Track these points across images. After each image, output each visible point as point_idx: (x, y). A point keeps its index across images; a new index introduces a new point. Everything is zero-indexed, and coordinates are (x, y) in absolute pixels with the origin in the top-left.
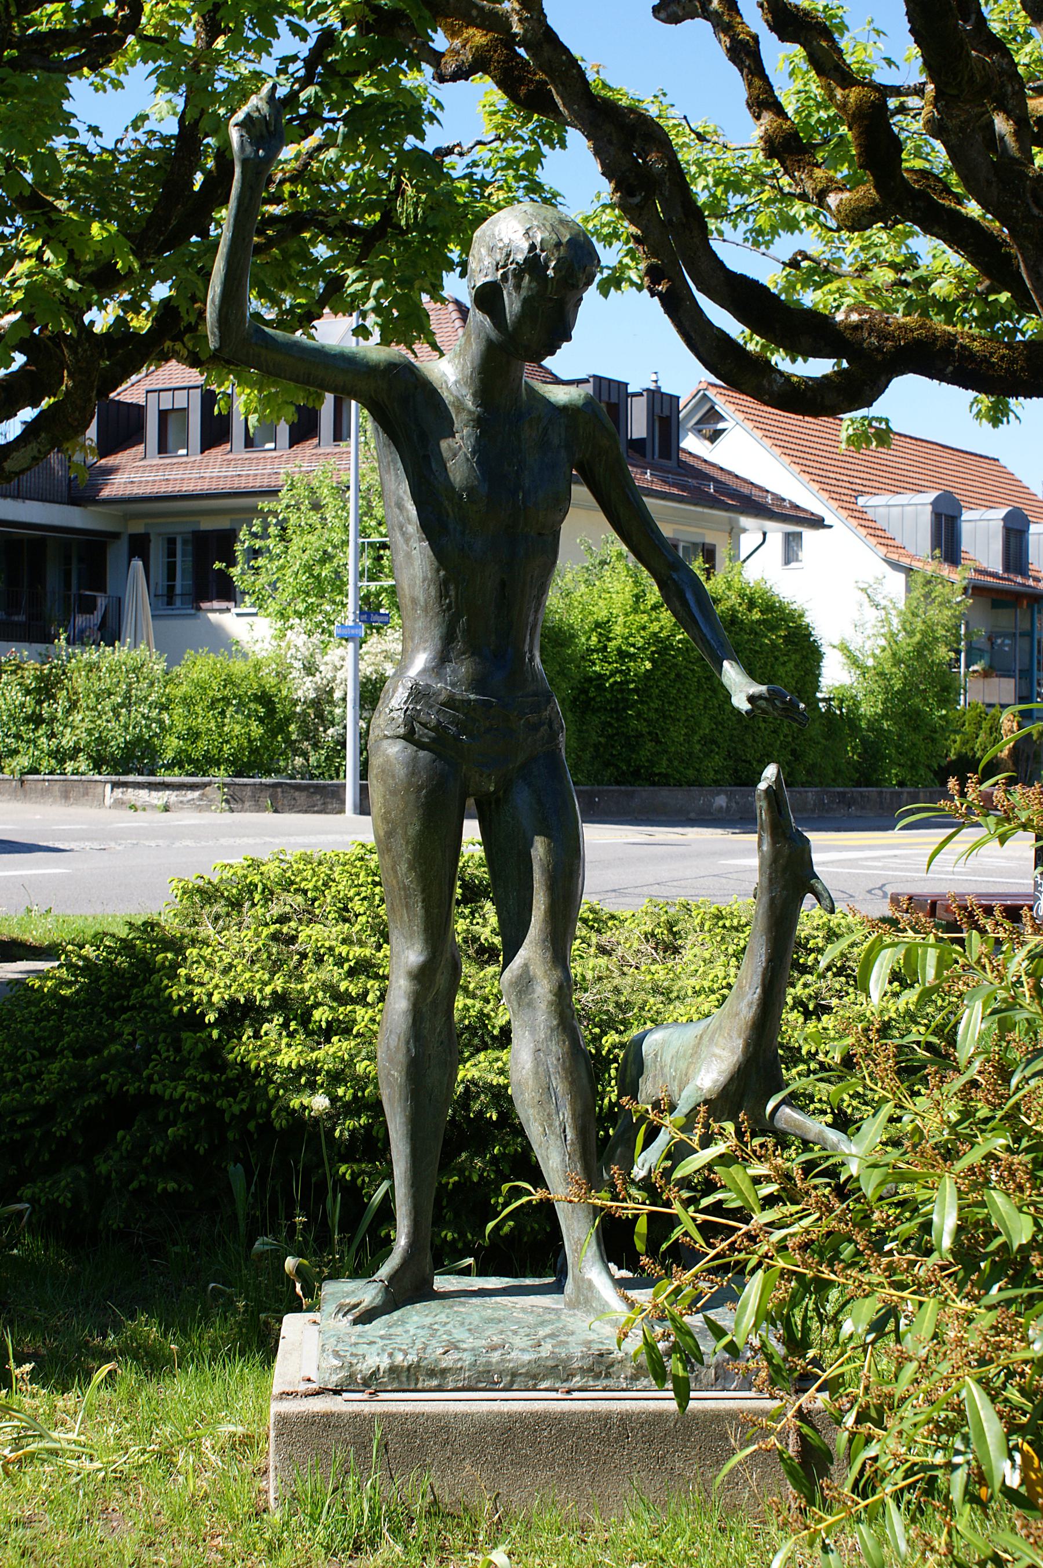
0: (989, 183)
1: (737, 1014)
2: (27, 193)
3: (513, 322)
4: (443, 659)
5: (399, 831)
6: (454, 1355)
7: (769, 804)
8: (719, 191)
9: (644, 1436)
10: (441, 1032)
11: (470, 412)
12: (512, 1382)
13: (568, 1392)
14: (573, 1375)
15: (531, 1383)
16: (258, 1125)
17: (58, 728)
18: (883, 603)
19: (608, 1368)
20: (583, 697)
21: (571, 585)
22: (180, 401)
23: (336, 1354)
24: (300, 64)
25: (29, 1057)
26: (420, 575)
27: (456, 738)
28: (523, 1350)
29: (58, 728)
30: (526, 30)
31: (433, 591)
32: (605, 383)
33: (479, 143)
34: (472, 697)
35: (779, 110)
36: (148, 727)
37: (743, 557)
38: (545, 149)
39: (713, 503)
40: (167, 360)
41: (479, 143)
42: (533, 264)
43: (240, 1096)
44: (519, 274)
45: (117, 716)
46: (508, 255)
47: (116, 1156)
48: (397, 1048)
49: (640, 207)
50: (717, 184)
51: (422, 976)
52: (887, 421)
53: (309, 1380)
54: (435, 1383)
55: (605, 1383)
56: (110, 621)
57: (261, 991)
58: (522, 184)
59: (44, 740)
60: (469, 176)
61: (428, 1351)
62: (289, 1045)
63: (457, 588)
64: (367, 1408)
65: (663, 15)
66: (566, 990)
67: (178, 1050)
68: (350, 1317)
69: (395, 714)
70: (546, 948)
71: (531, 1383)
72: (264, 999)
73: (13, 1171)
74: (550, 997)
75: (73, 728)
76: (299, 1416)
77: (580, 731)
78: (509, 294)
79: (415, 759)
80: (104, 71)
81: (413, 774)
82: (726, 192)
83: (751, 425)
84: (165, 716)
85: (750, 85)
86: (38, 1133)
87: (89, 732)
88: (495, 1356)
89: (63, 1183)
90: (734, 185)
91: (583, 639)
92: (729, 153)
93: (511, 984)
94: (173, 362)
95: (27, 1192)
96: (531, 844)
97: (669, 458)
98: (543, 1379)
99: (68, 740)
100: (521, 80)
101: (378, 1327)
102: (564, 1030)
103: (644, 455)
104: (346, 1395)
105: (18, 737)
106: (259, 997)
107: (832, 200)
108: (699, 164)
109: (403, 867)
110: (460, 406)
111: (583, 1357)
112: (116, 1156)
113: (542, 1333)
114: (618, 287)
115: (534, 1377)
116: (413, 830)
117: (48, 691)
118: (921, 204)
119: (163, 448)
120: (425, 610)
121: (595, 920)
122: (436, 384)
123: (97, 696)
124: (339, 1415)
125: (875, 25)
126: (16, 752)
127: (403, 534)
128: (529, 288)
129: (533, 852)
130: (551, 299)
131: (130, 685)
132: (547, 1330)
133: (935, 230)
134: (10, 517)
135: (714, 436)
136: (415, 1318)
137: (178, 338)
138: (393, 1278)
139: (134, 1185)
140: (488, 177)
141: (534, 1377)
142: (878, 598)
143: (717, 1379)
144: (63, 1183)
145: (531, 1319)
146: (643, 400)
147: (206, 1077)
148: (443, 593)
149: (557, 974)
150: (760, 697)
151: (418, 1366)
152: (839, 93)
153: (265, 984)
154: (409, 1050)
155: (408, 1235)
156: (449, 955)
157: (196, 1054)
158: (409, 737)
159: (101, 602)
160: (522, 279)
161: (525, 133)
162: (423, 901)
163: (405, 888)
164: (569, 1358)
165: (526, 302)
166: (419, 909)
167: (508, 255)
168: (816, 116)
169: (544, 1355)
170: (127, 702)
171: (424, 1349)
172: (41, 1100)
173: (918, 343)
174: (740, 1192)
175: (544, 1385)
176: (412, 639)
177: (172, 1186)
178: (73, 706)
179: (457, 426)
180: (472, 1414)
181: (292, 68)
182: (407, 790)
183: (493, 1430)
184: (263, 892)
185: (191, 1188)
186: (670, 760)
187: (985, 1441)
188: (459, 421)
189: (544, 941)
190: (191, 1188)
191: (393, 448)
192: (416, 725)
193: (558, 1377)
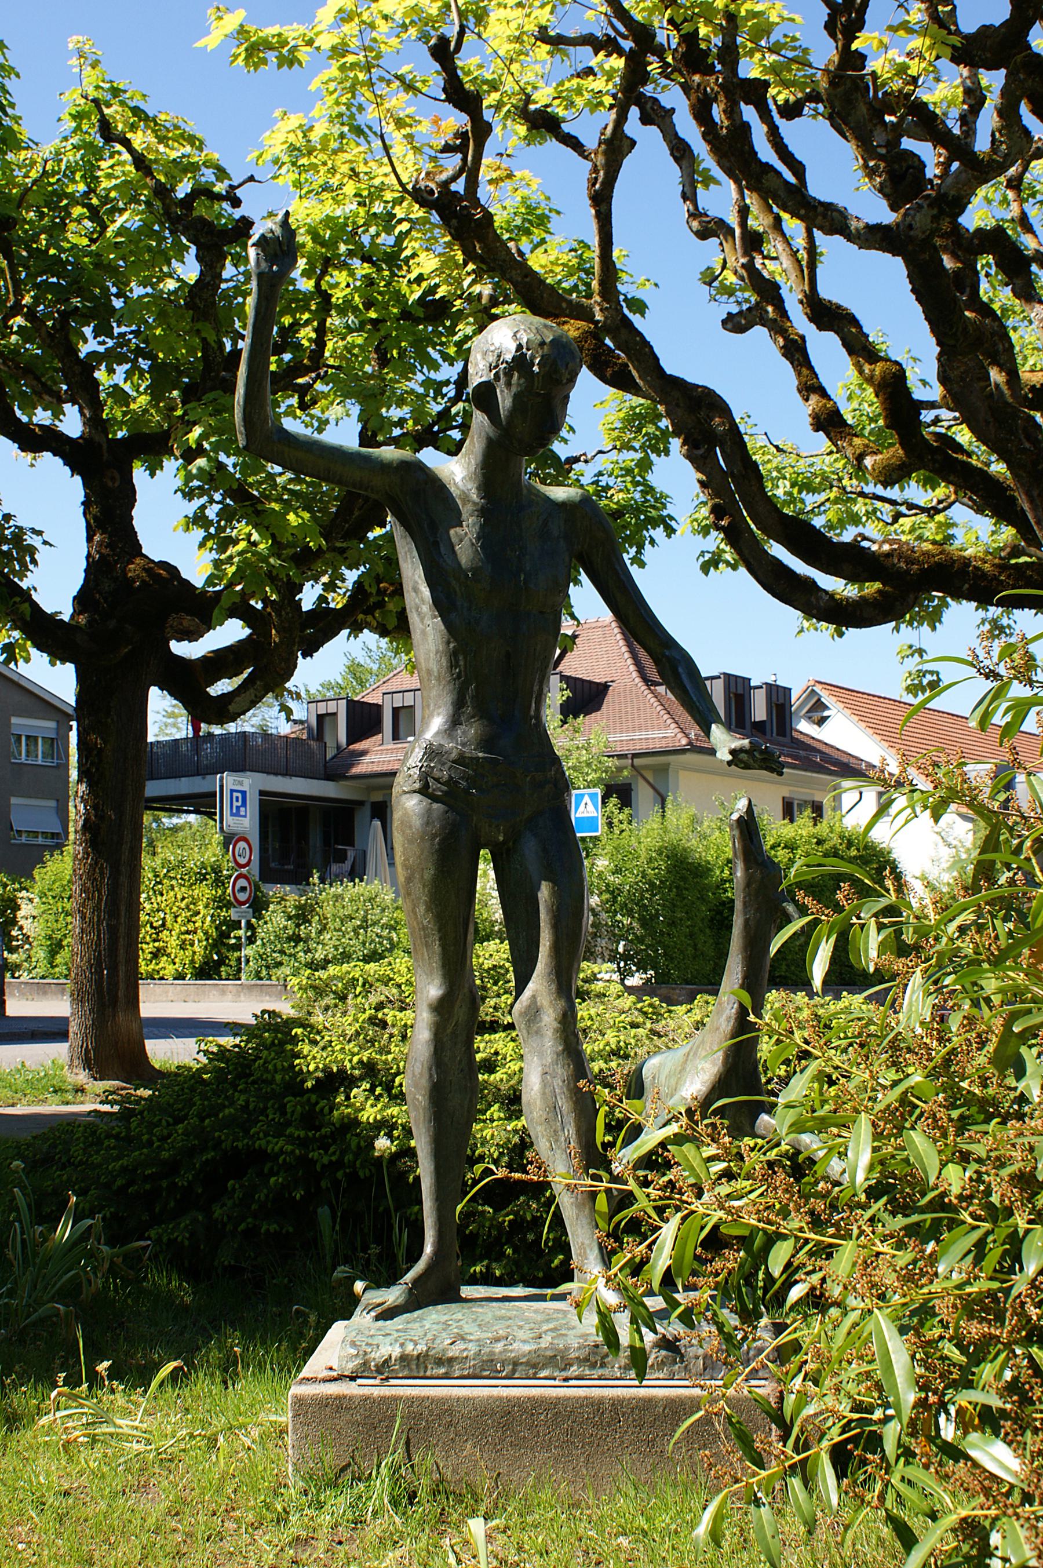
0: (987, 423)
1: (718, 1029)
2: (235, 486)
3: (507, 417)
4: (454, 722)
5: (417, 876)
6: (460, 1345)
7: (741, 833)
8: (795, 491)
9: (634, 1420)
10: (460, 1061)
11: (475, 504)
12: (514, 1371)
13: (566, 1379)
14: (571, 1365)
15: (531, 1372)
16: (345, 1174)
17: (312, 945)
18: (954, 843)
19: (603, 1358)
20: (718, 917)
21: (708, 831)
22: (332, 707)
23: (353, 1344)
24: (452, 386)
25: (164, 1123)
26: (433, 648)
27: (466, 791)
28: (524, 1341)
29: (312, 945)
30: (606, 318)
31: (444, 662)
32: (732, 679)
33: (601, 452)
34: (481, 755)
35: (823, 392)
36: (381, 943)
37: (845, 809)
38: (653, 457)
39: (820, 769)
40: (361, 631)
41: (601, 452)
42: (520, 362)
43: (332, 1150)
44: (509, 374)
45: (357, 934)
46: (499, 356)
47: (230, 1203)
48: (421, 1074)
49: (704, 457)
50: (793, 486)
51: (442, 1008)
52: (938, 674)
53: (331, 1369)
54: (442, 1371)
55: (601, 1372)
56: (357, 868)
57: (350, 1061)
58: (639, 488)
59: (301, 954)
60: (596, 483)
61: (438, 1341)
62: (372, 1106)
63: (465, 658)
64: (376, 1392)
65: (729, 326)
66: (570, 1019)
67: (283, 1113)
68: (373, 1314)
69: (411, 772)
70: (552, 981)
71: (531, 1372)
72: (353, 1068)
73: (145, 1217)
74: (556, 1025)
75: (324, 945)
76: (314, 1398)
77: (717, 944)
78: (502, 391)
79: (429, 811)
80: (312, 412)
81: (427, 824)
82: (800, 492)
83: (849, 712)
84: (394, 935)
85: (799, 374)
86: (164, 1184)
87: (336, 948)
88: (499, 1347)
89: (182, 1225)
90: (808, 487)
91: (718, 873)
92: (802, 461)
93: (521, 1014)
94: (366, 631)
95: (153, 1233)
96: (539, 888)
97: (784, 736)
98: (543, 1368)
99: (319, 955)
100: (607, 364)
101: (399, 1322)
102: (569, 1055)
103: (764, 733)
104: (359, 1381)
105: (282, 952)
106: (349, 1066)
107: (868, 461)
108: (778, 469)
109: (422, 908)
110: (466, 498)
111: (579, 1348)
112: (230, 1203)
113: (545, 1328)
114: (716, 568)
115: (534, 1366)
116: (428, 875)
117: (304, 916)
118: (938, 457)
119: (396, 737)
120: (438, 679)
121: (653, 1013)
122: (445, 481)
123: (342, 921)
124: (351, 1398)
125: (913, 354)
126: (281, 964)
127: (419, 614)
128: (519, 385)
129: (540, 895)
130: (539, 395)
131: (366, 911)
132: (551, 1326)
133: (951, 478)
134: (281, 790)
135: (821, 722)
136: (434, 1316)
137: (369, 611)
138: (416, 1282)
139: (242, 1227)
140: (611, 484)
141: (534, 1366)
142: (950, 839)
143: (705, 1369)
144: (182, 1225)
145: (539, 1318)
146: (763, 691)
147: (302, 1133)
148: (453, 664)
149: (561, 1004)
150: (741, 750)
151: (427, 1355)
152: (867, 368)
153: (353, 1055)
154: (431, 1076)
155: (433, 1244)
156: (466, 990)
157: (296, 1116)
158: (424, 791)
159: (351, 854)
160: (512, 376)
161: (637, 445)
162: (440, 939)
163: (424, 928)
164: (567, 1349)
165: (516, 397)
166: (437, 947)
167: (499, 356)
168: (868, 428)
169: (543, 1346)
170: (365, 924)
171: (433, 1340)
172: (165, 1155)
173: (939, 565)
174: (692, 1169)
175: (543, 1374)
176: (428, 706)
177: (274, 1227)
178: (324, 929)
179: (464, 516)
180: (474, 1399)
181: (445, 390)
182: (422, 838)
183: (493, 1414)
184: (364, 985)
185: (291, 1230)
186: (788, 965)
187: (893, 1373)
188: (466, 510)
189: (550, 973)
190: (291, 1230)
191: (409, 539)
192: (431, 782)
193: (557, 1366)
